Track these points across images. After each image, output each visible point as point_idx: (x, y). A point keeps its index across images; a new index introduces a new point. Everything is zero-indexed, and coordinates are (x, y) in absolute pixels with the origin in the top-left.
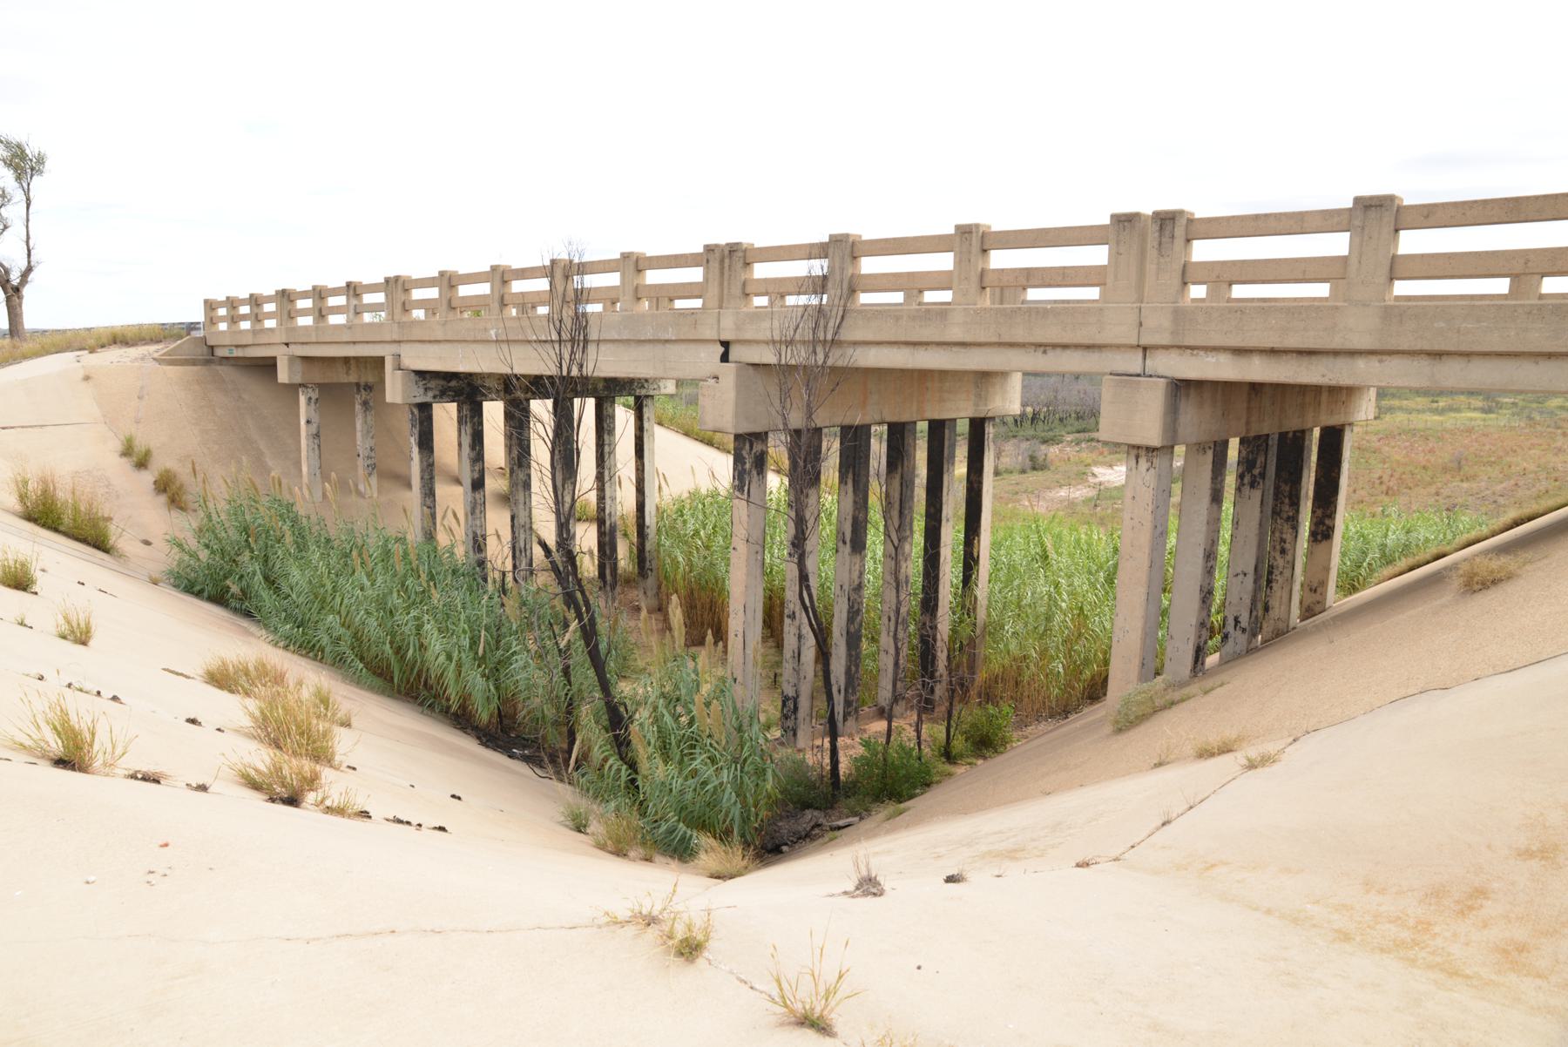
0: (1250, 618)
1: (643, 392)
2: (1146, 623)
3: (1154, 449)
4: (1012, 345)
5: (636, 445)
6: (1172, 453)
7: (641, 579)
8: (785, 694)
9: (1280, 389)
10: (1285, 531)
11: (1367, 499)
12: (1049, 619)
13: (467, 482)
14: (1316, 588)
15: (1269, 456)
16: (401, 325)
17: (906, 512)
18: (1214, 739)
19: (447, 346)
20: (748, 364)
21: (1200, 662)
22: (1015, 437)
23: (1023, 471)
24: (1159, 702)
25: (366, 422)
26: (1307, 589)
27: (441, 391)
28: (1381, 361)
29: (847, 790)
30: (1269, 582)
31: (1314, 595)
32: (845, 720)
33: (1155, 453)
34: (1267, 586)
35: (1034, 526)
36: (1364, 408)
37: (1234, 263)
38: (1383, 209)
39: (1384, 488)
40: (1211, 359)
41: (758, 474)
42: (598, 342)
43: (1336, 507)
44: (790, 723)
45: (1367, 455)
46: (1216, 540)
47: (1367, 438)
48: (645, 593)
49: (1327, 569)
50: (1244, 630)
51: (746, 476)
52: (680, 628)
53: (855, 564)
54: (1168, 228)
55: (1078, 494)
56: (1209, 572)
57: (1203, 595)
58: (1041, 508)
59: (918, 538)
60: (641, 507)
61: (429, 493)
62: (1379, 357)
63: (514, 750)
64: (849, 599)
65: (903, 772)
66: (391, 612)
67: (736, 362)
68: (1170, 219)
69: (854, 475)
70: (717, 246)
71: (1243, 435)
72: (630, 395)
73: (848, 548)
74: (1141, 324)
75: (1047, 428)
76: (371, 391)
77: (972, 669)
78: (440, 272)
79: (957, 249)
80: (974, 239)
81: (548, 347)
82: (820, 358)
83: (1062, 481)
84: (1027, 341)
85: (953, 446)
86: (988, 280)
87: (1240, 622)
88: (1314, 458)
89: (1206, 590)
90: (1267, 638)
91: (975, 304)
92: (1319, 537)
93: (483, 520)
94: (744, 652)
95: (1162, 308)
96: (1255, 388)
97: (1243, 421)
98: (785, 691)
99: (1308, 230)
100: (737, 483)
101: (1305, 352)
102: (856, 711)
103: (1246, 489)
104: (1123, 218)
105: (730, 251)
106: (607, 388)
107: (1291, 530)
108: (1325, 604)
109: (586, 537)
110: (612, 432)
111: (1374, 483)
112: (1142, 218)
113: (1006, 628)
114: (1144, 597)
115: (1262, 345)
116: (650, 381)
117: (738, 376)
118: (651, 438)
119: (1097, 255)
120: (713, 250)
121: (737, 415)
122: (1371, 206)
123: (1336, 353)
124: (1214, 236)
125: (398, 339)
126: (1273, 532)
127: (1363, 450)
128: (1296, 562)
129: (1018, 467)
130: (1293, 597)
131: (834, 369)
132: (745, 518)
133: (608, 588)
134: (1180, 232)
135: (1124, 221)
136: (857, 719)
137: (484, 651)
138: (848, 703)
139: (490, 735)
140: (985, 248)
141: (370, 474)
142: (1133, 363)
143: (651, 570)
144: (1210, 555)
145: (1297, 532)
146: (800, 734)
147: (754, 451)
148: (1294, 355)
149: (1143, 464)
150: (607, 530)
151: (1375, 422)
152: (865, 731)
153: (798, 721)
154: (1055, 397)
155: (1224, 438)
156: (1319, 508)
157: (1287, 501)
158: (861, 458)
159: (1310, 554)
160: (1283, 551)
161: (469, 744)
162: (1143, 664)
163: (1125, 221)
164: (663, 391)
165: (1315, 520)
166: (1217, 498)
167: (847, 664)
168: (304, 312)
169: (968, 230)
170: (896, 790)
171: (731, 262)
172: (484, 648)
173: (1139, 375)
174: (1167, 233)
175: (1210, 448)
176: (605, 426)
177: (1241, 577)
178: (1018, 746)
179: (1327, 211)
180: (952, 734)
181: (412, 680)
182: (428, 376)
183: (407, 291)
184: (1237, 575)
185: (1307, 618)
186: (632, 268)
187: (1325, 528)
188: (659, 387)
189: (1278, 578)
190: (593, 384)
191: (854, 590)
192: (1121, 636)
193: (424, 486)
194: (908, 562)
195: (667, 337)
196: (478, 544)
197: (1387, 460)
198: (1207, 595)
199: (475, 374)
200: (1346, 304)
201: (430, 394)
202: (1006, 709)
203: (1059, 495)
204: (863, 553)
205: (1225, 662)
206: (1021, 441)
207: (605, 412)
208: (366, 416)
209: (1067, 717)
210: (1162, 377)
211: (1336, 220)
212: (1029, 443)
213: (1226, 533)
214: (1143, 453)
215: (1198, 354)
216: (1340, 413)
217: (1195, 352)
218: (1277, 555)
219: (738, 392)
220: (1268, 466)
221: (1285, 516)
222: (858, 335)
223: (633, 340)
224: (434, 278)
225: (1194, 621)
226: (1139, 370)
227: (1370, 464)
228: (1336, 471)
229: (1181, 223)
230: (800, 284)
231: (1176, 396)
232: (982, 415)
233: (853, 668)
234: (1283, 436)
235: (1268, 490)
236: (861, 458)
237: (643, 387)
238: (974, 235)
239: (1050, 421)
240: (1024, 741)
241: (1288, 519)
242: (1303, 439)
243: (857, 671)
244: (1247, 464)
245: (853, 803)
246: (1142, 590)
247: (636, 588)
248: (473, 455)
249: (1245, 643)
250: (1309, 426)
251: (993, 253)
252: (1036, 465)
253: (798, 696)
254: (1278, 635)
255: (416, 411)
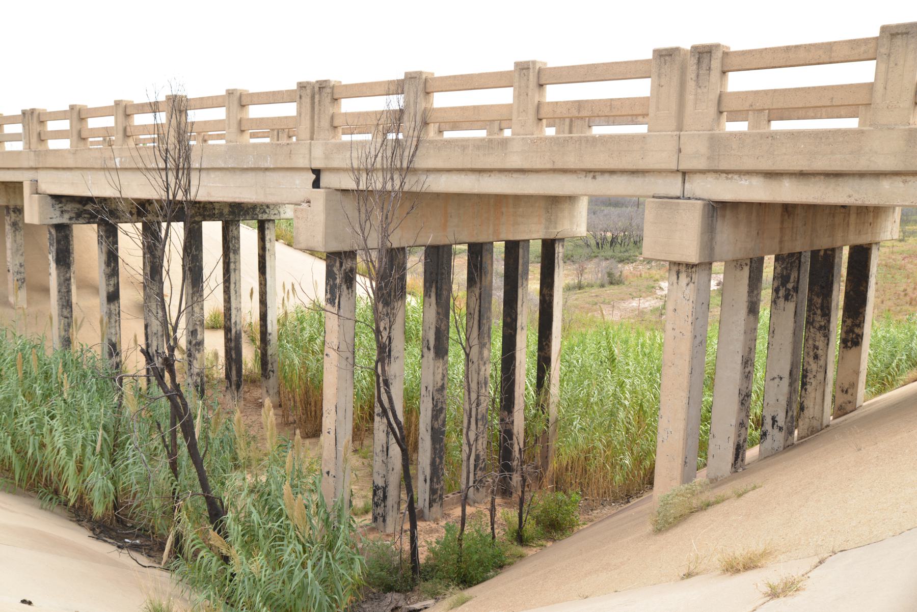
0: (786, 418)
1: (265, 217)
2: (687, 424)
3: (694, 266)
4: (565, 171)
5: (259, 262)
6: (710, 269)
7: (263, 379)
8: (376, 484)
9: (812, 209)
10: (817, 339)
11: (893, 308)
12: (613, 414)
13: (104, 295)
14: (847, 389)
15: (802, 272)
16: (37, 153)
17: (485, 321)
18: (740, 551)
19: (77, 173)
20: (337, 190)
21: (740, 459)
22: (596, 257)
23: (602, 286)
24: (695, 502)
25: (15, 241)
26: (839, 390)
27: (76, 213)
28: (905, 182)
29: (426, 574)
30: (804, 384)
31: (845, 395)
32: (431, 506)
33: (694, 270)
34: (802, 387)
35: (604, 333)
36: (889, 229)
37: (766, 92)
38: (909, 36)
39: (908, 299)
40: (744, 182)
41: (348, 288)
42: (200, 170)
43: (864, 317)
44: (380, 510)
45: (893, 271)
46: (753, 348)
47: (893, 257)
48: (267, 391)
49: (857, 373)
50: (781, 429)
51: (337, 290)
52: (272, 429)
53: (438, 367)
54: (705, 61)
55: (647, 305)
56: (747, 376)
57: (741, 398)
58: (613, 316)
59: (497, 343)
60: (263, 317)
61: (66, 304)
62: (904, 178)
63: (127, 540)
64: (433, 399)
65: (476, 557)
66: (16, 413)
67: (326, 188)
68: (706, 52)
69: (437, 289)
70: (308, 83)
71: (777, 252)
72: (253, 219)
73: (432, 354)
74: (680, 151)
75: (623, 250)
76: (20, 214)
77: (545, 458)
78: (70, 106)
79: (516, 84)
80: (531, 74)
81: (156, 174)
82: (397, 183)
83: (634, 294)
84: (578, 167)
85: (526, 264)
86: (543, 113)
87: (777, 421)
88: (844, 271)
89: (744, 393)
90: (803, 435)
91: (533, 134)
92: (849, 344)
93: (118, 328)
94: (336, 449)
95: (699, 135)
96: (788, 209)
97: (777, 240)
98: (375, 481)
99: (836, 60)
100: (329, 296)
101: (833, 174)
102: (441, 497)
103: (781, 302)
104: (664, 53)
105: (320, 88)
106: (232, 213)
107: (822, 338)
108: (856, 403)
109: (215, 342)
110: (237, 251)
111: (899, 295)
112: (682, 53)
113: (574, 423)
114: (685, 401)
115: (791, 168)
116: (272, 207)
117: (328, 200)
118: (272, 257)
119: (641, 88)
120: (305, 87)
121: (327, 235)
122: (898, 34)
123: (862, 175)
124: (748, 67)
125: (34, 166)
126: (806, 340)
127: (890, 267)
128: (828, 367)
129: (599, 282)
130: (826, 398)
131: (405, 193)
132: (336, 328)
133: (233, 387)
134: (716, 64)
135: (665, 56)
136: (441, 505)
137: (102, 448)
138: (433, 491)
139: (105, 526)
140: (541, 83)
141: (20, 288)
142: (673, 186)
143: (273, 371)
144: (748, 362)
145: (828, 339)
146: (389, 520)
147: (344, 267)
148: (822, 177)
149: (684, 279)
150: (233, 338)
151: (899, 244)
152: (449, 515)
153: (387, 509)
154: (631, 224)
155: (759, 255)
156: (849, 318)
157: (819, 312)
158: (442, 274)
159: (841, 359)
160: (816, 357)
161: (79, 537)
162: (686, 462)
163: (666, 55)
164: (283, 216)
165: (845, 328)
166: (753, 309)
167: (432, 458)
168: (59, 135)
169: (526, 66)
170: (470, 573)
171: (320, 97)
172: (102, 445)
173: (678, 198)
174: (704, 65)
175: (746, 264)
176: (231, 246)
177: (777, 380)
178: (583, 529)
179: (855, 40)
180: (524, 519)
181: (33, 476)
182: (63, 200)
183: (42, 122)
184: (773, 379)
185: (840, 416)
186: (236, 103)
187: (854, 336)
188: (279, 212)
189: (812, 381)
190: (220, 209)
191: (437, 390)
192: (665, 437)
193: (61, 299)
194: (487, 365)
195: (266, 166)
196: (113, 349)
197: (911, 275)
198: (745, 398)
199: (110, 198)
200: (872, 128)
201: (66, 216)
202: (575, 497)
203: (631, 305)
204: (445, 358)
205: (764, 457)
206: (601, 260)
207: (231, 234)
208: (15, 236)
209: (628, 502)
210: (699, 199)
211: (863, 48)
212: (608, 262)
213: (761, 345)
214: (683, 269)
215: (732, 177)
216: (867, 234)
217: (730, 176)
218: (811, 360)
219: (328, 214)
220: (800, 280)
221: (817, 325)
222: (430, 163)
223: (238, 168)
224: (65, 111)
225: (733, 422)
226: (679, 194)
227: (896, 279)
228: (864, 285)
229: (718, 55)
230: (378, 118)
231: (712, 217)
232: (552, 237)
233: (438, 460)
234: (815, 254)
235: (802, 302)
236: (442, 274)
237: (265, 212)
238: (531, 71)
239: (626, 244)
240: (590, 524)
241: (820, 328)
242: (834, 257)
243: (441, 463)
244: (782, 279)
245: (430, 586)
246: (684, 395)
247: (260, 387)
248: (108, 271)
249: (782, 441)
250: (839, 244)
251: (549, 88)
252: (613, 280)
253: (386, 486)
254: (812, 433)
255: (53, 231)
